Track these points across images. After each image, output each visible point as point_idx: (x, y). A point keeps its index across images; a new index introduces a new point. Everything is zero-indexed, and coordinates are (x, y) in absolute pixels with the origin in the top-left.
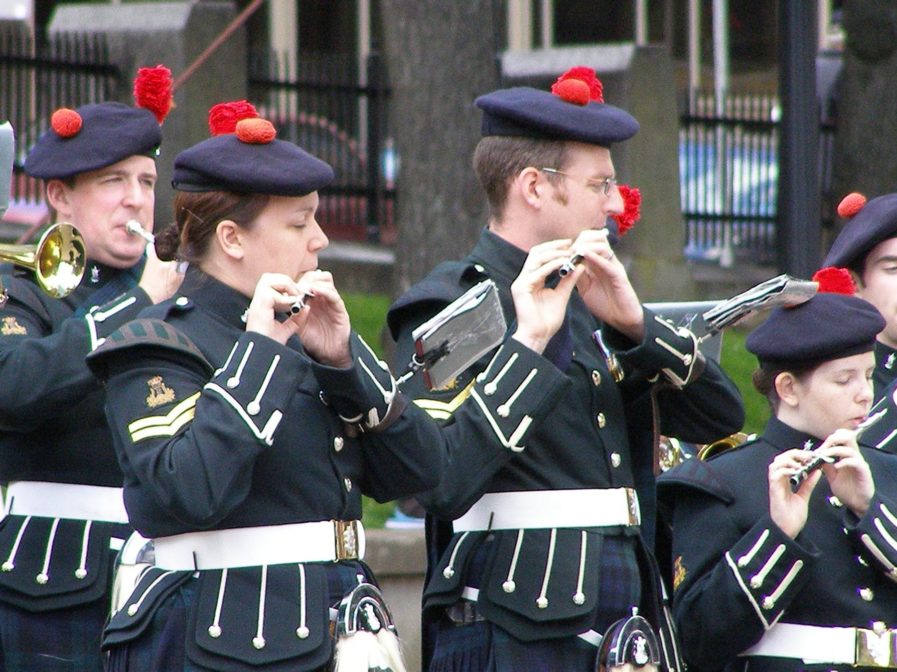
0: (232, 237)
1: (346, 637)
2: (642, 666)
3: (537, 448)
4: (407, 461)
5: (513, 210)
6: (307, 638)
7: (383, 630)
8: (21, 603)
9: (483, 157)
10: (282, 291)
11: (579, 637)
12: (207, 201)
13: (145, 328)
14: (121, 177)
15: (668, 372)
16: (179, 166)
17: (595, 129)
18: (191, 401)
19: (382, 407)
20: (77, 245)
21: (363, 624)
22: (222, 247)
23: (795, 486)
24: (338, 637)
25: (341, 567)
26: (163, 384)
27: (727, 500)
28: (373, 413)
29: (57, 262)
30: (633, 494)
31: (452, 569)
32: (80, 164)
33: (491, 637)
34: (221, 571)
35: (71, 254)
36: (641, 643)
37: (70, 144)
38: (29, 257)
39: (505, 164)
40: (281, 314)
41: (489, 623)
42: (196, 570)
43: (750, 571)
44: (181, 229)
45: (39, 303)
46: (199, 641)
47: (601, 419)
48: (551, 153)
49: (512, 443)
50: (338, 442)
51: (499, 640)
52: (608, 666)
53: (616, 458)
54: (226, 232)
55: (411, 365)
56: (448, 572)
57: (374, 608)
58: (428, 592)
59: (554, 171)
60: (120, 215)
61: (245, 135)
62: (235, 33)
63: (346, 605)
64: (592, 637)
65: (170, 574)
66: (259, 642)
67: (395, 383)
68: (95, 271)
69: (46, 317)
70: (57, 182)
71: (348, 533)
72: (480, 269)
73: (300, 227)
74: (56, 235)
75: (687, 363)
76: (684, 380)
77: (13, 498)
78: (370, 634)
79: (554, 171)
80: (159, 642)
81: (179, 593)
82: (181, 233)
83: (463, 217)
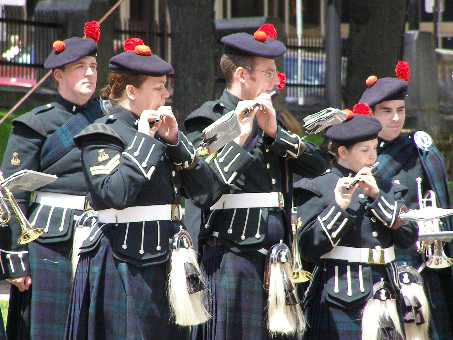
2: (283, 263)
7: (189, 248)
13: (98, 126)
22: (127, 95)
23: (345, 190)
26: (104, 152)
28: (186, 164)
31: (208, 225)
37: (61, 54)
40: (152, 123)
42: (117, 223)
43: (326, 223)
44: (111, 87)
48: (249, 61)
50: (174, 174)
57: (186, 239)
64: (263, 251)
65: (105, 225)
71: (176, 209)
75: (296, 148)
78: (185, 249)
82: (111, 89)
83: (199, 84)
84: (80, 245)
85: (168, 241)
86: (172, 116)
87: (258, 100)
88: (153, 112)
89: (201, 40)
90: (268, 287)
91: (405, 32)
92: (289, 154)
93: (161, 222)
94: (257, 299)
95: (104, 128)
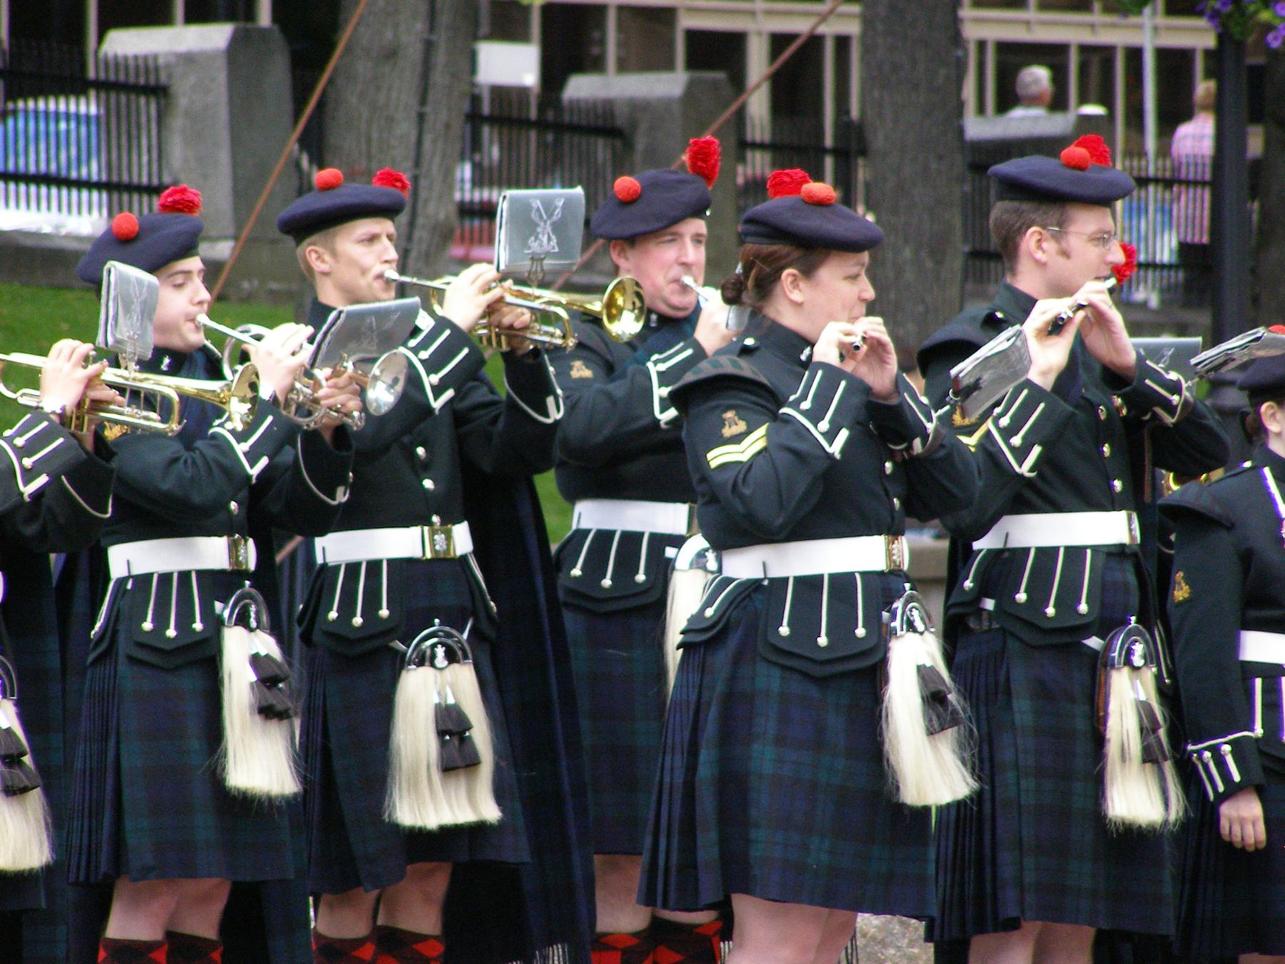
0: (795, 283)
1: (897, 638)
2: (1138, 668)
3: (1049, 473)
4: (946, 483)
5: (1024, 266)
6: (1084, 615)
8: (590, 606)
9: (996, 219)
10: (848, 334)
11: (1085, 645)
12: (771, 254)
14: (676, 238)
15: (1159, 411)
16: (750, 221)
17: (1091, 191)
18: (762, 430)
19: (925, 436)
20: (639, 295)
21: (911, 627)
24: (890, 637)
25: (893, 578)
27: (1228, 525)
29: (620, 310)
30: (1135, 516)
32: (641, 228)
33: (1005, 642)
34: (787, 579)
35: (634, 303)
36: (1139, 649)
38: (596, 305)
39: (1013, 225)
41: (1003, 630)
44: (747, 277)
45: (604, 347)
46: (773, 640)
47: (1106, 449)
48: (1054, 213)
49: (1025, 469)
50: (888, 465)
51: (1012, 645)
52: (1108, 668)
53: (1118, 484)
54: (790, 279)
55: (948, 399)
56: (968, 584)
58: (950, 602)
59: (1057, 229)
60: (675, 271)
61: (811, 197)
62: (727, 122)
63: (897, 608)
64: (1094, 642)
66: (823, 641)
67: (935, 415)
68: (654, 317)
69: (609, 357)
70: (619, 242)
72: (999, 315)
73: (854, 278)
74: (620, 287)
75: (1175, 403)
76: (1173, 418)
77: (324, 549)
78: (917, 635)
79: (1057, 229)
80: (733, 642)
81: (751, 598)
83: (929, 264)
84: (683, 624)
85: (881, 616)
86: (886, 338)
87: (1081, 297)
88: (847, 326)
89: (934, 166)
90: (1104, 720)
91: (1068, 207)
92: (1155, 416)
93: (865, 574)
94: (1082, 747)
95: (734, 363)
